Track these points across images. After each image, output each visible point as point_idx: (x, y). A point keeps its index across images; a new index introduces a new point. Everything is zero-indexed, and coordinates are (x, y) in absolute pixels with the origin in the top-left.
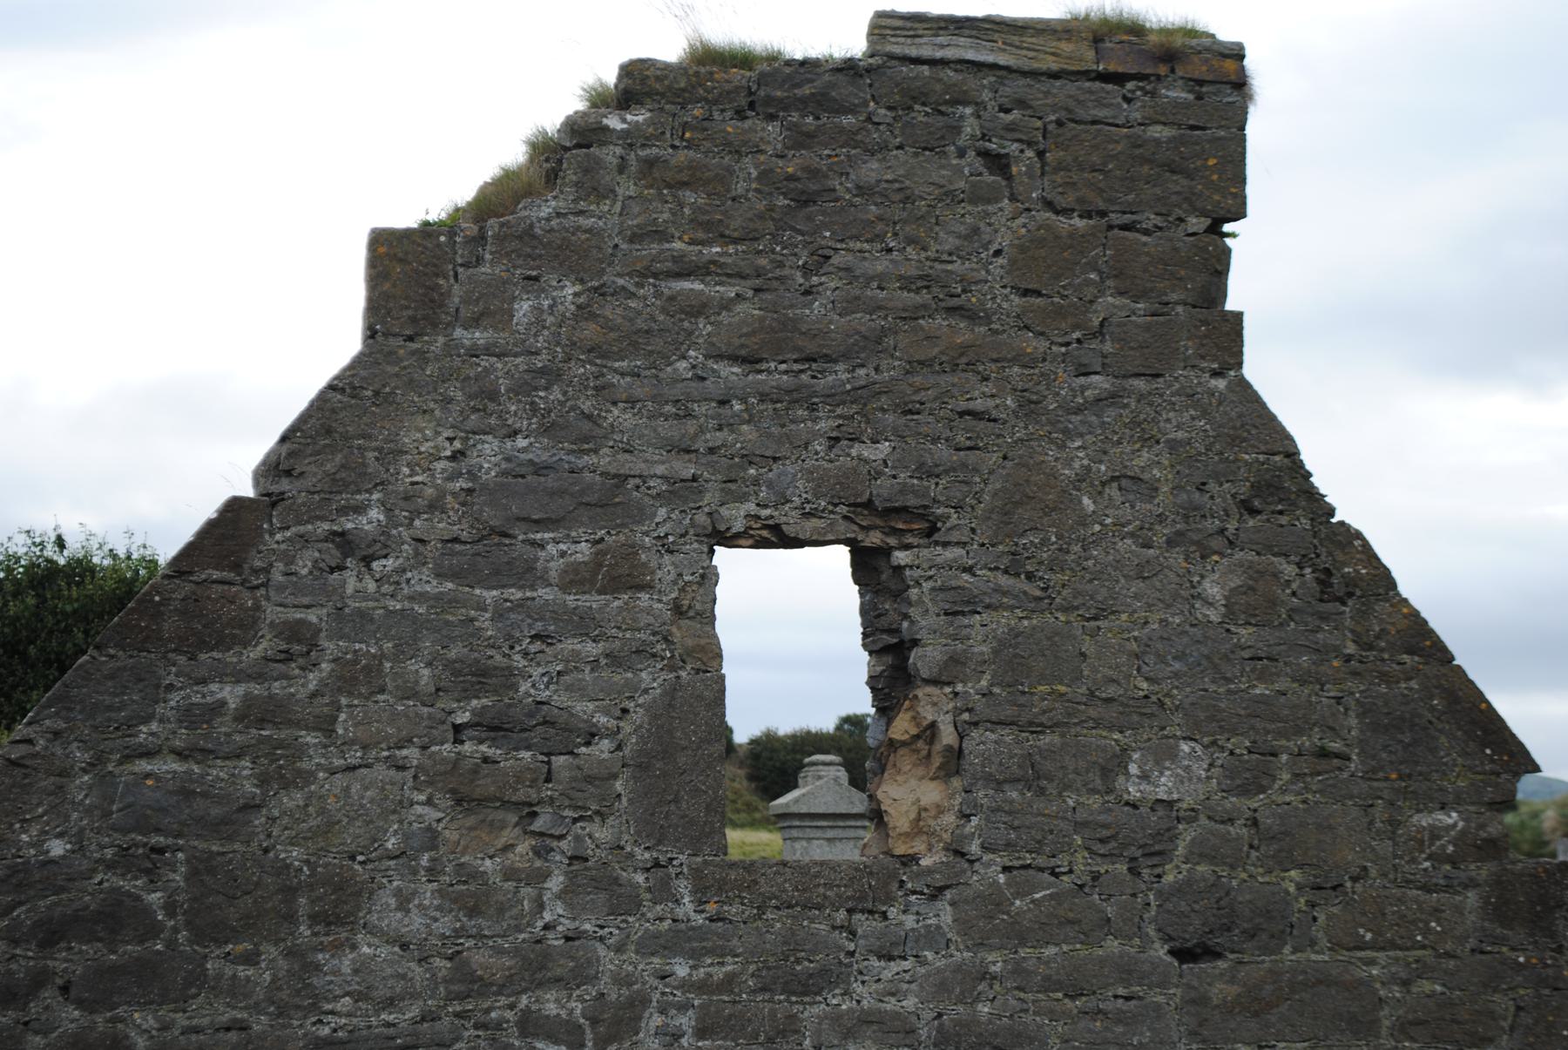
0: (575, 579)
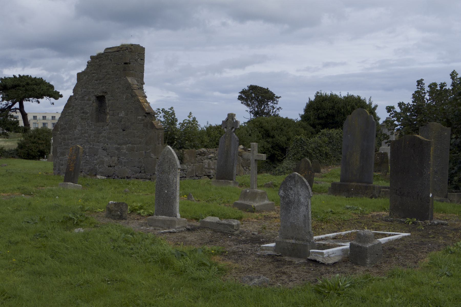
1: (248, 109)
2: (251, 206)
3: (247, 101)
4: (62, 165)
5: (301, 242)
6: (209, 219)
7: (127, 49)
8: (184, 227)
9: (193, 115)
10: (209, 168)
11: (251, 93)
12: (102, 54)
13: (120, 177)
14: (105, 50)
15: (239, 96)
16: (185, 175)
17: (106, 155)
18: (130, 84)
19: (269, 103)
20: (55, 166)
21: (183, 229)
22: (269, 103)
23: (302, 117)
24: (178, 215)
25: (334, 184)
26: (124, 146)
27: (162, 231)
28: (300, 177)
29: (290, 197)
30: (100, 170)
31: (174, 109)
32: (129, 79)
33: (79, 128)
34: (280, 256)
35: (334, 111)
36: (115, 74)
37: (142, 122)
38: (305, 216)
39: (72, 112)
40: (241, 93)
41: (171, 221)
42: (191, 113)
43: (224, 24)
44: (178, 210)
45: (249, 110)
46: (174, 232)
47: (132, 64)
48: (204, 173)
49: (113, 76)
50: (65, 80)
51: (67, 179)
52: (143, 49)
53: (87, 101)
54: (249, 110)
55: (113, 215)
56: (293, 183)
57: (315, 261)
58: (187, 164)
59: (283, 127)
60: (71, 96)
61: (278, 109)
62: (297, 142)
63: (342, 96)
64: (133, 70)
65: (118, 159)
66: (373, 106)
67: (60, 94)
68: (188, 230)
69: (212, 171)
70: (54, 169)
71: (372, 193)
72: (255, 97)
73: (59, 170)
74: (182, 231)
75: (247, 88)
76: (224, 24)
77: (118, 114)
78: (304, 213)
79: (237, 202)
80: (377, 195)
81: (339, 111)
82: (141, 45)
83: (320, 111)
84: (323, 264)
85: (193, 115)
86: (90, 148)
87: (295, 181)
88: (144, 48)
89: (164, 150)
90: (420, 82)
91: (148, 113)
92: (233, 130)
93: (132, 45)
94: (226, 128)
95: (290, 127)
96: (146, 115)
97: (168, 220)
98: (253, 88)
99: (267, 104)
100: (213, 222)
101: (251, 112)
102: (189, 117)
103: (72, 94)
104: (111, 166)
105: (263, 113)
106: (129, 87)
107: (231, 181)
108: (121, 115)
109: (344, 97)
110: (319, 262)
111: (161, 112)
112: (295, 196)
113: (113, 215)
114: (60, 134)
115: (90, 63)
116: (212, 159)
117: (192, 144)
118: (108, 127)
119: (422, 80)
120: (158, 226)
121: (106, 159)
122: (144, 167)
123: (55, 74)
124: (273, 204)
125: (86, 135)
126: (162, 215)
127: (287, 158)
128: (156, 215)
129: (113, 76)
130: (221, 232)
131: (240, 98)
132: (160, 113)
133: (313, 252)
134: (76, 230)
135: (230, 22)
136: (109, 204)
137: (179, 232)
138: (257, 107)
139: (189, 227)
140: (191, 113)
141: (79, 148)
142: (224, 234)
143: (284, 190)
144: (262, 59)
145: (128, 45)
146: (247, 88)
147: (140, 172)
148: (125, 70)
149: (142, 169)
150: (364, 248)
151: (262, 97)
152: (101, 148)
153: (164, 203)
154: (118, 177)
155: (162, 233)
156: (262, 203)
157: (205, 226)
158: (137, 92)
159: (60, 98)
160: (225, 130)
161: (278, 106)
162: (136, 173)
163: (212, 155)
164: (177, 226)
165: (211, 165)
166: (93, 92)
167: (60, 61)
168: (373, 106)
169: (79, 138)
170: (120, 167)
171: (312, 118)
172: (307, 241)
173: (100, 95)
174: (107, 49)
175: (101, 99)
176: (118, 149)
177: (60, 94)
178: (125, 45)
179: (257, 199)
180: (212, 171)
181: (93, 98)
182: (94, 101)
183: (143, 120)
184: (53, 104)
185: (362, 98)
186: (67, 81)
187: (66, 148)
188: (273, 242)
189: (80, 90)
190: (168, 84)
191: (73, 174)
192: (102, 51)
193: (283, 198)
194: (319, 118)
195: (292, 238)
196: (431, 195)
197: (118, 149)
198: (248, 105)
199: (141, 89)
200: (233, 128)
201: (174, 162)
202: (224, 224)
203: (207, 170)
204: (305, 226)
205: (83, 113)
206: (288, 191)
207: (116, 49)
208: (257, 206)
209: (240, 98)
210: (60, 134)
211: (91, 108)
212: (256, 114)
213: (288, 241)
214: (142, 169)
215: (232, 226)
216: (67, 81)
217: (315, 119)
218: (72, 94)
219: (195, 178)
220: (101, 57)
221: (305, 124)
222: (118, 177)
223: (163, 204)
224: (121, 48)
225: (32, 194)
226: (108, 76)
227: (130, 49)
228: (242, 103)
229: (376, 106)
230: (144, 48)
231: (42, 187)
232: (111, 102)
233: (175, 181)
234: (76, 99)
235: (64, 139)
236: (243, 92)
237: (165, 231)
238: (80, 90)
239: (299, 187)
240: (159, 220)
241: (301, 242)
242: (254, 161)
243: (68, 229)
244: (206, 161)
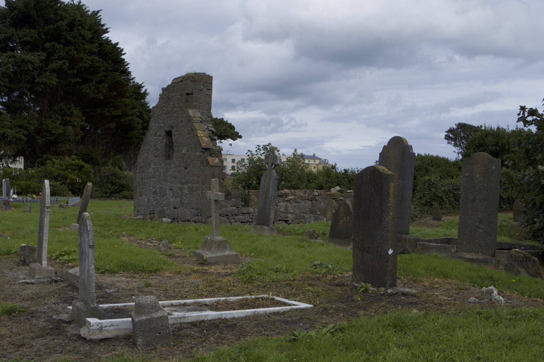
2: (203, 256)
7: (189, 78)
8: (48, 277)
10: (286, 212)
14: (173, 80)
15: (446, 136)
18: (190, 117)
21: (45, 280)
26: (185, 186)
32: (191, 112)
33: (152, 166)
35: (498, 148)
37: (200, 159)
43: (451, 60)
47: (195, 95)
48: (279, 218)
50: (284, 123)
52: (210, 78)
58: (254, 207)
59: (429, 167)
63: (510, 130)
64: (197, 101)
67: (239, 134)
70: (135, 211)
71: (402, 247)
72: (464, 137)
74: (43, 283)
75: (455, 127)
76: (451, 60)
80: (410, 250)
81: (503, 148)
86: (160, 188)
88: (212, 77)
92: (273, 166)
93: (196, 74)
96: (203, 151)
98: (462, 126)
107: (266, 227)
109: (513, 131)
111: (262, 149)
116: (291, 201)
117: (290, 185)
121: (172, 200)
123: (275, 117)
125: (158, 174)
132: (260, 150)
135: (457, 57)
144: (495, 97)
145: (191, 74)
146: (455, 127)
149: (199, 211)
156: (220, 254)
159: (238, 139)
163: (291, 197)
164: (37, 277)
165: (289, 209)
167: (278, 104)
169: (153, 178)
175: (169, 134)
176: (181, 189)
177: (239, 134)
179: (213, 249)
181: (163, 134)
183: (200, 156)
184: (231, 145)
186: (287, 124)
188: (133, 302)
190: (390, 125)
192: (170, 83)
196: (390, 252)
197: (181, 189)
200: (273, 164)
207: (180, 79)
208: (209, 258)
209: (447, 137)
214: (199, 211)
216: (287, 124)
218: (236, 130)
220: (169, 89)
226: (175, 109)
227: (193, 77)
228: (448, 143)
230: (212, 77)
232: (176, 136)
236: (451, 131)
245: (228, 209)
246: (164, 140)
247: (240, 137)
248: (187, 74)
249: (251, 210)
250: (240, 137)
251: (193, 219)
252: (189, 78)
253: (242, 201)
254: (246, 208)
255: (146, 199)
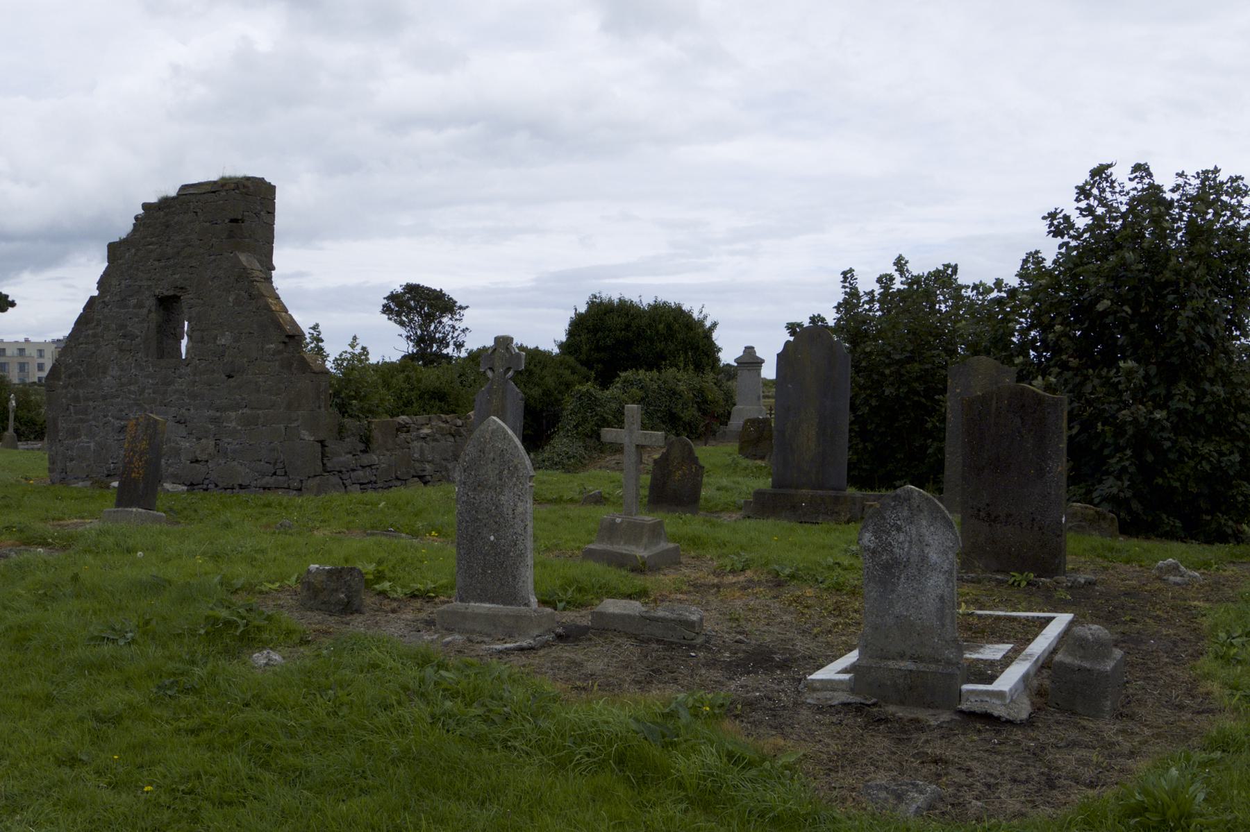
0: (135, 307)
1: (403, 332)
3: (399, 314)
4: (71, 460)
5: (933, 667)
6: (613, 606)
7: (238, 188)
9: (361, 342)
11: (409, 299)
12: (173, 198)
13: (221, 485)
16: (374, 478)
17: (185, 434)
18: (245, 268)
19: (445, 320)
20: (52, 461)
21: (550, 637)
22: (445, 320)
23: (561, 346)
24: (533, 600)
25: (759, 494)
26: (233, 414)
27: (499, 647)
28: (927, 499)
29: (896, 550)
30: (171, 470)
31: (320, 328)
32: (243, 258)
33: (114, 371)
34: (874, 704)
35: (630, 334)
36: (200, 248)
38: (942, 598)
39: (94, 335)
40: (387, 298)
41: (518, 618)
42: (355, 338)
44: (531, 586)
45: (405, 333)
46: (531, 648)
48: (412, 472)
49: (202, 251)
51: (126, 498)
53: (135, 307)
54: (405, 333)
55: (324, 603)
56: (906, 513)
57: (987, 718)
60: (92, 298)
61: (463, 331)
62: (580, 398)
65: (216, 444)
66: (708, 324)
67: (10, 299)
68: (560, 637)
69: (428, 467)
70: (51, 470)
73: (64, 471)
77: (215, 338)
78: (939, 592)
79: (592, 546)
82: (268, 180)
83: (600, 334)
84: (1010, 722)
85: (361, 342)
87: (910, 508)
89: (482, 427)
90: (847, 275)
91: (291, 337)
92: (511, 373)
93: (248, 179)
94: (490, 368)
95: (544, 367)
97: (507, 616)
98: (412, 289)
99: (440, 322)
100: (629, 616)
101: (408, 337)
102: (352, 346)
103: (96, 293)
104: (197, 461)
105: (433, 340)
106: (243, 275)
108: (223, 341)
110: (999, 718)
112: (910, 548)
113: (324, 603)
114: (65, 387)
115: (142, 219)
118: (189, 369)
119: (851, 270)
120: (473, 631)
122: (283, 462)
124: (677, 549)
125: (132, 388)
126: (481, 601)
127: (561, 433)
128: (462, 600)
129: (202, 251)
130: (658, 641)
131: (386, 310)
133: (973, 692)
134: (259, 658)
136: (309, 572)
137: (543, 647)
138: (420, 327)
139: (560, 630)
140: (355, 338)
141: (156, 421)
142: (670, 646)
143: (875, 533)
147: (275, 474)
148: (231, 236)
150: (1100, 673)
151: (430, 306)
152: (170, 418)
153: (487, 568)
154: (217, 486)
155: (500, 652)
157: (605, 628)
158: (262, 286)
159: (10, 309)
160: (490, 374)
161: (462, 325)
162: (264, 475)
166: (150, 286)
168: (708, 324)
170: (222, 462)
171: (585, 348)
172: (949, 662)
173: (166, 293)
174: (184, 187)
176: (214, 420)
178: (231, 179)
180: (428, 467)
181: (151, 302)
182: (153, 309)
183: (280, 352)
185: (686, 308)
187: (81, 420)
189: (114, 282)
191: (141, 486)
193: (874, 552)
194: (598, 349)
195: (902, 656)
197: (214, 420)
198: (402, 324)
199: (269, 279)
200: (509, 369)
201: (516, 461)
202: (663, 620)
203: (417, 464)
204: (943, 625)
205: (124, 336)
206: (888, 534)
207: (209, 188)
209: (386, 310)
210: (65, 387)
211: (146, 325)
212: (419, 341)
213: (891, 664)
215: (690, 625)
217: (590, 349)
218: (96, 293)
219: (395, 483)
221: (571, 360)
222: (217, 486)
223: (484, 572)
224: (223, 186)
225: (49, 544)
227: (244, 186)
229: (715, 325)
230: (271, 189)
231: (59, 519)
233: (520, 509)
234: (106, 304)
235: (76, 399)
236: (393, 297)
237: (508, 645)
238: (114, 282)
239: (924, 523)
240: (476, 616)
241: (933, 667)
242: (634, 449)
243: (229, 653)
244: (417, 444)
245: (342, 459)
246: (153, 316)
247: (13, 304)
248: (223, 179)
249: (374, 458)
250: (13, 304)
251: (259, 483)
252: (238, 188)
253: (361, 441)
254: (366, 456)
255: (92, 445)
